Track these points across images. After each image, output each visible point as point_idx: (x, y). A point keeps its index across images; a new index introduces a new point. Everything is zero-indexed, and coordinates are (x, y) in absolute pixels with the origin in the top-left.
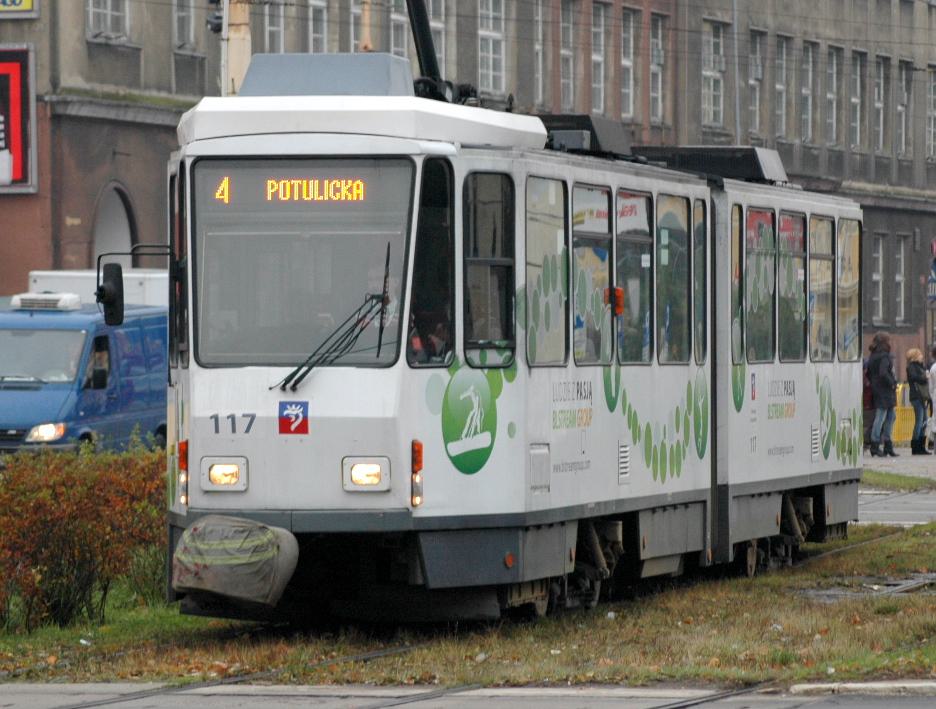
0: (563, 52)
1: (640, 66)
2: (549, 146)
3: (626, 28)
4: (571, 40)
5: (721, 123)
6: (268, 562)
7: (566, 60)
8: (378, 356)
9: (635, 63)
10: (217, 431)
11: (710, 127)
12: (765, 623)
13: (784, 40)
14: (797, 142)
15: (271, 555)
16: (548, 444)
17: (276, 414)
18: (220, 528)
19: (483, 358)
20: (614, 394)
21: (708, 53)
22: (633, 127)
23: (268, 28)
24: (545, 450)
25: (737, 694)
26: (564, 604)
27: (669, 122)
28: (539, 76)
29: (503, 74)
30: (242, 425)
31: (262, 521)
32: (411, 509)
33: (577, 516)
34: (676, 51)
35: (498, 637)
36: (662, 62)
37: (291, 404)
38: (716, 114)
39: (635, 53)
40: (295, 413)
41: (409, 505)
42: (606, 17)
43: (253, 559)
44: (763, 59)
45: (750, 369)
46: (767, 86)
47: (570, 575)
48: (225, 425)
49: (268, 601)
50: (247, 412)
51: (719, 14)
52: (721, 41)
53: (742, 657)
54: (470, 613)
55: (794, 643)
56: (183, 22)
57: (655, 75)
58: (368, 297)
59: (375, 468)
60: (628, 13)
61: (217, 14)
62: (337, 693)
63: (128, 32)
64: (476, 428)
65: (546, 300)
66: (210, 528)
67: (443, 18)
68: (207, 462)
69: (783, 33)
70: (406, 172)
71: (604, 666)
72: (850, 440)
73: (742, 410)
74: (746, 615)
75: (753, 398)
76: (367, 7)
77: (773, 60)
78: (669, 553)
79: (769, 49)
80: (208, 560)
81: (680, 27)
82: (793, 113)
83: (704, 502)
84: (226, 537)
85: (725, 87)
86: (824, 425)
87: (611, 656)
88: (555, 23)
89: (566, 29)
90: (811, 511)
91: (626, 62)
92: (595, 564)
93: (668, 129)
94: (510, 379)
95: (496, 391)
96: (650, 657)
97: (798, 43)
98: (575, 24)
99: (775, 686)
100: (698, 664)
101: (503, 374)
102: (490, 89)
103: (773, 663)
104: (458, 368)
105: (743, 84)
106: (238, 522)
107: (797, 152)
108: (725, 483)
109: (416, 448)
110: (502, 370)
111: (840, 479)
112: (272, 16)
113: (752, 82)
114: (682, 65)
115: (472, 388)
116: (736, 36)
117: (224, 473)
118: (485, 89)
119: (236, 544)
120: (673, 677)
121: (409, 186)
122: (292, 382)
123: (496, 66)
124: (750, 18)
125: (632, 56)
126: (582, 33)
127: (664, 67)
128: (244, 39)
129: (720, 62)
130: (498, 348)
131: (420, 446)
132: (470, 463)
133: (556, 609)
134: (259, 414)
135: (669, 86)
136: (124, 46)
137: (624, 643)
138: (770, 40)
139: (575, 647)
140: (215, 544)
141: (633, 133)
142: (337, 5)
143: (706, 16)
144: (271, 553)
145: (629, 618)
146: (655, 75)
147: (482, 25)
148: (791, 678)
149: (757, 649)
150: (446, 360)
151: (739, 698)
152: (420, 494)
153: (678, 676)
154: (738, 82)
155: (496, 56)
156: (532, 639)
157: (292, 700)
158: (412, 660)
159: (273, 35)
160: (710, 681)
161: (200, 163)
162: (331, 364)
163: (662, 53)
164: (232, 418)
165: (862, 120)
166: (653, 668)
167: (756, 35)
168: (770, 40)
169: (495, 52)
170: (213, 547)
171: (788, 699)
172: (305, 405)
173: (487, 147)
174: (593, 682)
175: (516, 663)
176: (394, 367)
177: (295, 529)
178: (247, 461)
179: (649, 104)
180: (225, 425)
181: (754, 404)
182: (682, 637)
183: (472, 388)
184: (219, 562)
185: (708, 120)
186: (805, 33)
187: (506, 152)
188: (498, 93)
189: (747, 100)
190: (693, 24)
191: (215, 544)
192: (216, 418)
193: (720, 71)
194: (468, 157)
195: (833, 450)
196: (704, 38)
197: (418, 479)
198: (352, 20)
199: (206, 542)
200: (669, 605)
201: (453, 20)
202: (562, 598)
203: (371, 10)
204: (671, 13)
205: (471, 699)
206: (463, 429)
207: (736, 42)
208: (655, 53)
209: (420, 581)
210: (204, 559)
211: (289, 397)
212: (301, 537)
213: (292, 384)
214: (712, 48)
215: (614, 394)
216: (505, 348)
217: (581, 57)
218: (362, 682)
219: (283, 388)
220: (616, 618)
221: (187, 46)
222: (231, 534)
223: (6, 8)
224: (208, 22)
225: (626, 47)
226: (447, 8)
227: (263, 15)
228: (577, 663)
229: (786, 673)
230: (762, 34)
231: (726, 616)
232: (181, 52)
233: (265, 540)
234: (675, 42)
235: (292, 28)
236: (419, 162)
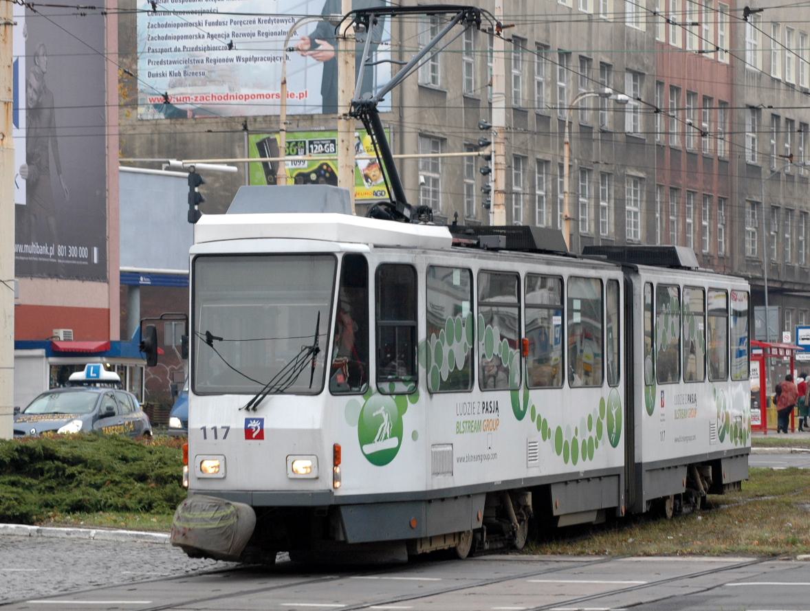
0: (671, 218)
1: (712, 225)
2: (455, 245)
3: (705, 205)
4: (675, 211)
5: (756, 255)
6: (230, 527)
7: (673, 222)
8: (310, 387)
9: (710, 224)
10: (205, 438)
11: (750, 257)
12: (782, 522)
13: (789, 211)
14: (797, 265)
15: (232, 522)
16: (452, 444)
17: (243, 426)
18: (200, 503)
19: (392, 388)
20: (522, 409)
21: (749, 218)
22: (709, 258)
23: (514, 206)
24: (449, 448)
25: (768, 560)
26: (483, 548)
27: (728, 255)
28: (659, 231)
29: (639, 230)
30: (221, 433)
31: (226, 499)
32: (332, 490)
33: (688, 462)
34: (731, 217)
35: (639, 530)
36: (724, 223)
37: (253, 420)
38: (753, 250)
39: (709, 218)
40: (255, 425)
41: (331, 487)
42: (694, 200)
43: (222, 525)
44: (778, 222)
45: (659, 388)
46: (781, 235)
47: (683, 494)
48: (210, 434)
49: (230, 553)
50: (224, 425)
51: (754, 197)
52: (756, 212)
53: (770, 540)
54: (387, 558)
55: (798, 533)
56: (470, 204)
57: (720, 230)
58: (304, 348)
59: (308, 463)
60: (706, 197)
61: (488, 199)
62: (555, 559)
63: (441, 210)
64: (386, 434)
65: (451, 347)
66: (194, 504)
67: (607, 200)
68: (199, 459)
69: (789, 207)
70: (331, 263)
71: (697, 546)
72: (741, 430)
73: (588, 416)
74: (772, 518)
75: (662, 406)
76: (566, 195)
77: (784, 221)
78: (583, 510)
79: (781, 216)
80: (192, 525)
81: (734, 204)
82: (795, 249)
83: (619, 475)
84: (204, 510)
85: (758, 236)
86: (720, 421)
87: (700, 540)
88: (667, 202)
89: (673, 206)
90: (711, 475)
91: (705, 223)
92: (697, 488)
93: (728, 258)
94: (414, 402)
95: (402, 409)
96: (721, 541)
97: (797, 212)
98: (677, 203)
99: (790, 556)
100: (747, 544)
101: (408, 399)
102: (633, 238)
103: (787, 543)
104: (371, 395)
105: (767, 234)
106: (213, 499)
107: (797, 270)
108: (639, 461)
109: (337, 449)
110: (407, 396)
111: (733, 454)
112: (516, 200)
113: (772, 233)
114: (735, 226)
115: (383, 408)
116: (764, 209)
117: (210, 466)
118: (630, 238)
119: (211, 514)
120: (733, 551)
121: (333, 273)
122: (253, 405)
123: (636, 225)
124: (771, 199)
125: (708, 220)
126: (681, 207)
127: (725, 225)
128: (501, 212)
129: (755, 223)
130: (404, 381)
131: (340, 448)
132: (381, 459)
133: (476, 551)
134: (232, 426)
135: (728, 235)
136: (438, 217)
137: (707, 533)
138: (782, 211)
139: (681, 535)
140: (197, 514)
141: (709, 261)
142: (551, 194)
143: (747, 198)
144: (233, 521)
145: (709, 519)
146: (720, 230)
147: (628, 204)
148: (797, 551)
149: (778, 536)
150: (362, 390)
151: (769, 562)
152: (340, 481)
153: (737, 550)
154: (765, 233)
155: (636, 220)
156: (657, 531)
157: (531, 563)
158: (594, 542)
159: (516, 209)
160: (753, 553)
161: (198, 259)
162: (282, 392)
163: (724, 218)
164: (215, 429)
165: (806, 249)
166: (723, 547)
167: (775, 208)
168: (782, 211)
169: (634, 218)
170: (196, 517)
171: (796, 563)
172: (261, 421)
173: (398, 247)
174: (691, 554)
175: (649, 543)
176: (319, 396)
177: (255, 504)
178: (225, 458)
179: (717, 246)
180: (210, 434)
181: (663, 410)
182: (738, 530)
183: (383, 408)
184: (199, 527)
185: (749, 254)
186: (801, 207)
187: (411, 250)
188: (637, 239)
189: (770, 243)
190: (741, 203)
191: (197, 514)
192: (204, 429)
193: (755, 228)
194: (380, 253)
195: (727, 436)
196: (747, 210)
197: (338, 470)
198: (22, 115)
199: (191, 513)
200: (731, 513)
201: (612, 201)
202: (680, 507)
203: (569, 196)
204: (729, 197)
205: (625, 562)
206: (375, 436)
207: (764, 213)
208: (721, 217)
209: (342, 538)
210: (189, 525)
211: (252, 415)
212: (258, 510)
213: (253, 406)
214: (751, 216)
215: (522, 409)
216: (410, 381)
217: (681, 219)
218: (567, 554)
219: (247, 409)
220: (702, 520)
221: (472, 216)
222: (207, 508)
223: (377, 197)
224: (483, 203)
225: (705, 214)
226: (609, 195)
227: (511, 199)
228: (682, 543)
229: (795, 549)
230: (778, 208)
231: (762, 518)
232: (469, 219)
233: (229, 512)
234: (731, 212)
235: (527, 206)
236: (340, 258)
